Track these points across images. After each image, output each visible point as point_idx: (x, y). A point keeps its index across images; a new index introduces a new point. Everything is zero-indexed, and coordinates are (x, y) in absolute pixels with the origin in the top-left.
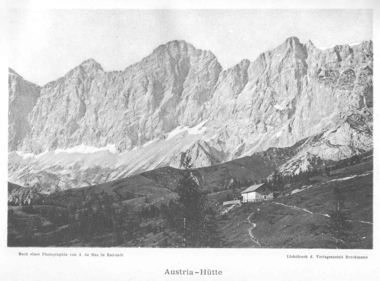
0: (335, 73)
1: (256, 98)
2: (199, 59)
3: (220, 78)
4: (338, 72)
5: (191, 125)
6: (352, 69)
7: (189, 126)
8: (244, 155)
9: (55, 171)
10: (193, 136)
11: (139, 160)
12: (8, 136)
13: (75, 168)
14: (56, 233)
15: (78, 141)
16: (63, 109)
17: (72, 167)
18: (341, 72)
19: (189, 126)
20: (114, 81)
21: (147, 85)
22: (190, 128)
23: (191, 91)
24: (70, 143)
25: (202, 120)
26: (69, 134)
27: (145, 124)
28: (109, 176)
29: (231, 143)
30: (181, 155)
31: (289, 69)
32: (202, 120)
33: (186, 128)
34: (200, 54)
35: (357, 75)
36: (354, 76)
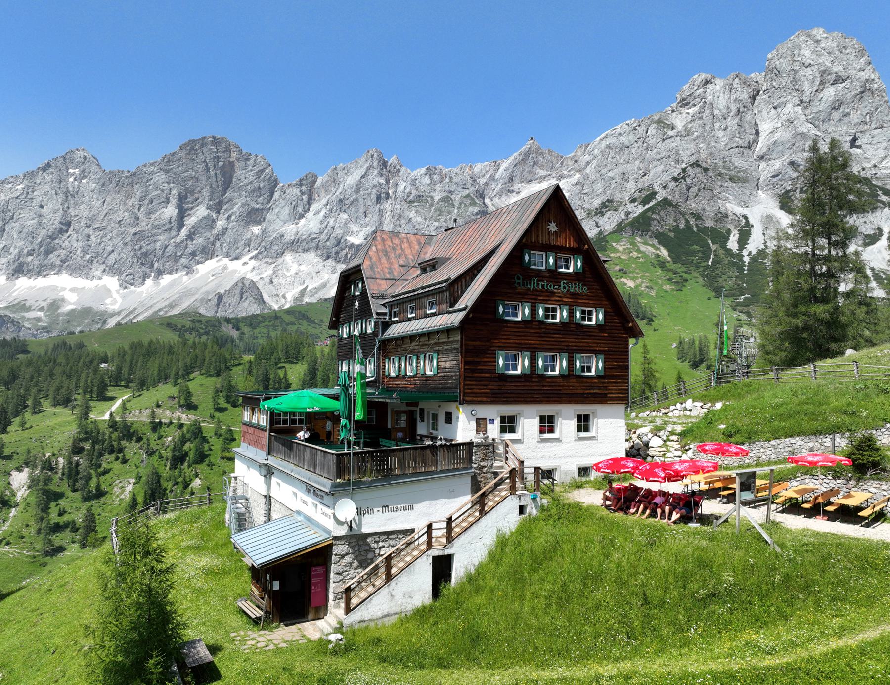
0: (429, 199)
1: (324, 225)
2: (246, 165)
3: (276, 195)
4: (432, 198)
5: (234, 256)
6: (450, 195)
7: (231, 258)
8: (306, 300)
9: (15, 312)
10: (234, 271)
11: (156, 301)
12: (110, 278)
13: (48, 310)
14: (765, 276)
15: (57, 269)
16: (33, 219)
17: (46, 308)
18: (436, 198)
19: (231, 258)
20: (117, 185)
21: (170, 194)
22: (232, 260)
23: (235, 209)
24: (40, 271)
25: (249, 251)
26: (42, 257)
27: (164, 251)
28: (105, 322)
29: (680, 394)
30: (216, 297)
31: (370, 190)
32: (249, 251)
33: (226, 261)
34: (249, 159)
35: (456, 204)
36: (453, 205)
